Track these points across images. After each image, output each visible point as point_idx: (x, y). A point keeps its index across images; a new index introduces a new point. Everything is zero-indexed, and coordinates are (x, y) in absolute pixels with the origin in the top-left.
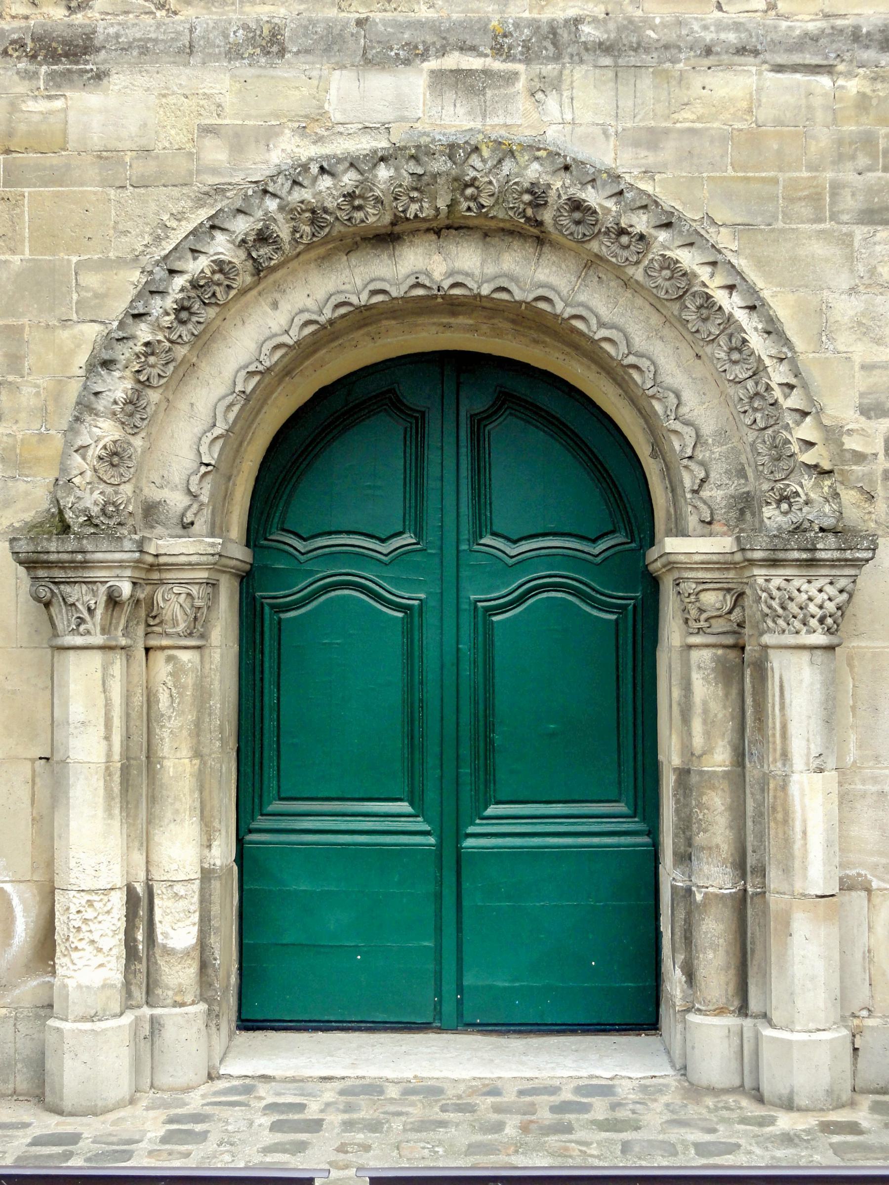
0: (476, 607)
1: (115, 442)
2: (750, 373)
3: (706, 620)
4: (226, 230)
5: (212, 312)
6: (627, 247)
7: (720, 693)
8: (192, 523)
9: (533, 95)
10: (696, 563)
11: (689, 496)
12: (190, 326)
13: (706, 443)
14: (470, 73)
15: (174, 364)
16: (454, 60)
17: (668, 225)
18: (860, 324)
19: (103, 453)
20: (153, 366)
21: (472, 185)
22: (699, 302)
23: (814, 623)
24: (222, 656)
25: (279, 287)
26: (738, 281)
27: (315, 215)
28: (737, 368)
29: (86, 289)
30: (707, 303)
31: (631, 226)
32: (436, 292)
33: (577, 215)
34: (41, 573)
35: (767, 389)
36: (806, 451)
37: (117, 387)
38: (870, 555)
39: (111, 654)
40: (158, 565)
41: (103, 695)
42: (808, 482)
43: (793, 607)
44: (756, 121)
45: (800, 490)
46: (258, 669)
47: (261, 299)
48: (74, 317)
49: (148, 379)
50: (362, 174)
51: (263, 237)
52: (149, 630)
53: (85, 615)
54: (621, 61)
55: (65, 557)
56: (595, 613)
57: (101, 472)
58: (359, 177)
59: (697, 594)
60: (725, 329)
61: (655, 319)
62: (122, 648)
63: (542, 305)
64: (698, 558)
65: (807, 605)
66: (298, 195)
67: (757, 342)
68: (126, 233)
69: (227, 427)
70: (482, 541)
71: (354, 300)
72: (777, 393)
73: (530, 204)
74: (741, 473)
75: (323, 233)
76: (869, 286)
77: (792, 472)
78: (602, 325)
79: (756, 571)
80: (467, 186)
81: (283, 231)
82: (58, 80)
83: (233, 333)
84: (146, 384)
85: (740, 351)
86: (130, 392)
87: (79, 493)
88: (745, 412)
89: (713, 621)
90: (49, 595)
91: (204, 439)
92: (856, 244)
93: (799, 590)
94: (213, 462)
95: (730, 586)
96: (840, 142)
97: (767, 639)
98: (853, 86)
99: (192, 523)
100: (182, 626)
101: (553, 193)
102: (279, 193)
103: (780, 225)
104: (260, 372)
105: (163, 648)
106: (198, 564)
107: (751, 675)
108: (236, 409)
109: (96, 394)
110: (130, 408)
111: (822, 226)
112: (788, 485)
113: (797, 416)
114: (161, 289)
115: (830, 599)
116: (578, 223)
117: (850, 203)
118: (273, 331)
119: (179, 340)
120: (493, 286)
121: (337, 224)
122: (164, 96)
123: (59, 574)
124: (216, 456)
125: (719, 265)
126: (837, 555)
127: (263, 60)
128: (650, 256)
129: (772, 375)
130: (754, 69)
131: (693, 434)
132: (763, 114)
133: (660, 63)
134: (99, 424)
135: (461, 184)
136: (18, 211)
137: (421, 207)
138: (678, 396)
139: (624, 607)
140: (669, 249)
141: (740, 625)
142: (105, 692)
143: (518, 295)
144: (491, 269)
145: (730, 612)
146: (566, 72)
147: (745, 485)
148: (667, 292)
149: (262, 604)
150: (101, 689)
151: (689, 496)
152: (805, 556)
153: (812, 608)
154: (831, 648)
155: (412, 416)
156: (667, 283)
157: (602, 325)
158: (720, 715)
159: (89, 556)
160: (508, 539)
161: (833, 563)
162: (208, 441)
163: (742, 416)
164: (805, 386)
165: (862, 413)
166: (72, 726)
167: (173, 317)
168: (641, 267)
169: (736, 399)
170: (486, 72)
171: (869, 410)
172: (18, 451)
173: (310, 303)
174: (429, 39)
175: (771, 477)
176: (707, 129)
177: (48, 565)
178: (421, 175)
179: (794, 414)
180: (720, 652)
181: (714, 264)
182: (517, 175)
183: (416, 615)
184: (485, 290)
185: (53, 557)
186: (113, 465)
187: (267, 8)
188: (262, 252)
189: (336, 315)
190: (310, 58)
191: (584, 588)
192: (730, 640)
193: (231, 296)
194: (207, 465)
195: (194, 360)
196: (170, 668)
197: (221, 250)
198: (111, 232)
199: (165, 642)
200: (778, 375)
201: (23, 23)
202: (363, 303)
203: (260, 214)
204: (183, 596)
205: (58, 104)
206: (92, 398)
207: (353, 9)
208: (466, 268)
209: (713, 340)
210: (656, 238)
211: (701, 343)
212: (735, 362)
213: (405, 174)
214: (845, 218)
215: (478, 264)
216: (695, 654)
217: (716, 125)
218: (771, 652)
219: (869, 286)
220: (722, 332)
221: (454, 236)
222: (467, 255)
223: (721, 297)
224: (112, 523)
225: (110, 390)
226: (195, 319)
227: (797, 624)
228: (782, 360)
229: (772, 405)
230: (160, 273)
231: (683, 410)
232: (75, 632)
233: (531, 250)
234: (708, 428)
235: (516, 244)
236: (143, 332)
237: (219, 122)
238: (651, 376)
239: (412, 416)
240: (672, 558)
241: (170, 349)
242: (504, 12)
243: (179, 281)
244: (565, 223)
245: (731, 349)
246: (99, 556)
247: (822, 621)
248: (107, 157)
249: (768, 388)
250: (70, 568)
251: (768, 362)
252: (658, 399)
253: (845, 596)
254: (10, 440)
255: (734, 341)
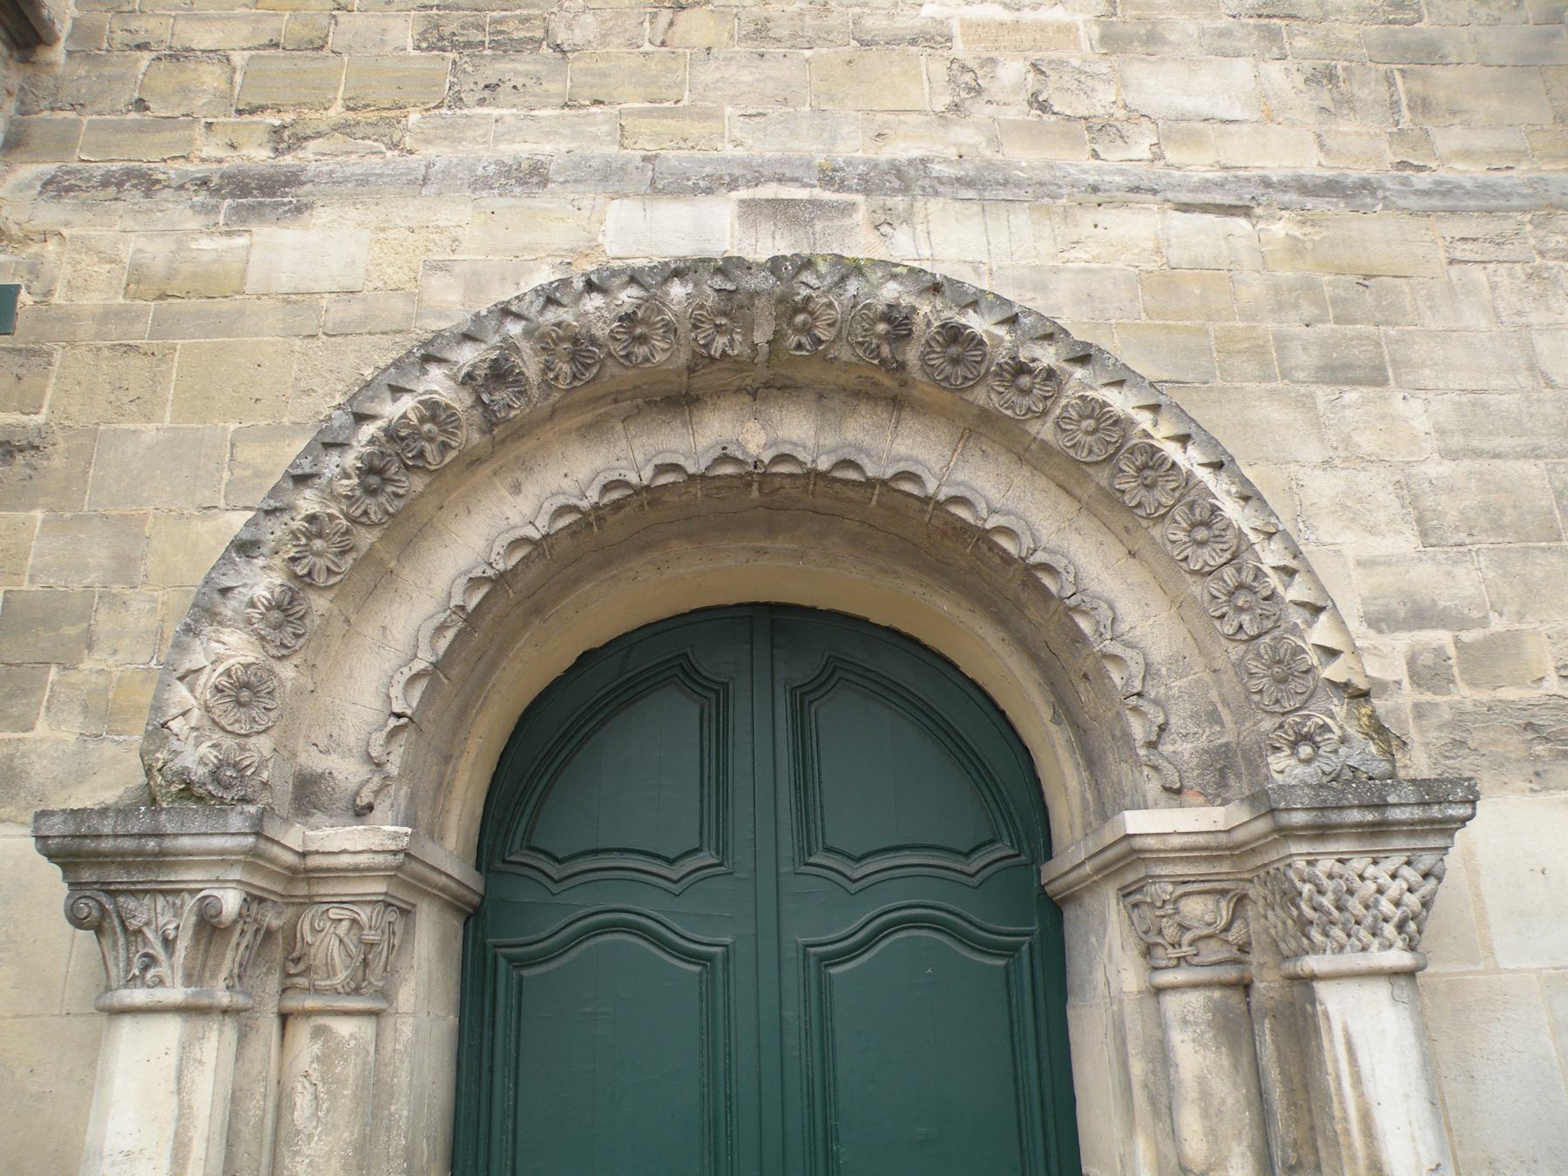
0: (805, 954)
1: (247, 666)
2: (1228, 555)
3: (1192, 943)
4: (445, 361)
5: (418, 483)
6: (1026, 392)
7: (1226, 1063)
8: (370, 808)
9: (877, 227)
10: (1174, 850)
11: (1142, 752)
12: (382, 499)
13: (1158, 674)
14: (791, 203)
15: (354, 555)
16: (768, 191)
17: (1083, 359)
18: (1345, 507)
19: (224, 681)
20: (318, 554)
21: (804, 310)
22: (1140, 460)
23: (1389, 930)
24: (416, 1031)
25: (524, 464)
26: (1193, 430)
27: (579, 346)
28: (1205, 553)
29: (245, 466)
30: (1152, 463)
31: (1034, 360)
32: (751, 469)
33: (954, 350)
34: (87, 876)
35: (1256, 578)
36: (1328, 663)
37: (262, 582)
38: (1469, 811)
39: (200, 1023)
40: (307, 871)
41: (175, 1099)
42: (1340, 708)
43: (1354, 905)
44: (1168, 263)
45: (1329, 721)
46: (486, 1053)
47: (496, 480)
48: (222, 504)
49: (309, 574)
50: (647, 290)
51: (500, 373)
52: (288, 982)
53: (158, 950)
54: (987, 195)
55: (128, 844)
56: (965, 953)
57: (217, 711)
58: (642, 293)
59: (1176, 901)
60: (1182, 495)
61: (1066, 505)
62: (225, 1011)
63: (908, 487)
64: (1177, 841)
65: (1377, 901)
66: (552, 315)
67: (1231, 509)
68: (308, 392)
69: (433, 659)
70: (812, 860)
71: (633, 478)
72: (1274, 580)
73: (886, 337)
74: (1214, 717)
75: (588, 376)
76: (1346, 459)
77: (1311, 696)
78: (993, 511)
79: (1295, 848)
80: (797, 310)
81: (530, 365)
82: (246, 215)
83: (453, 527)
84: (306, 581)
85: (1207, 525)
86: (278, 590)
87: (176, 745)
88: (1222, 616)
89: (1202, 945)
90: (95, 913)
91: (398, 677)
92: (1321, 407)
93: (1362, 877)
94: (409, 712)
95: (1224, 885)
96: (1276, 289)
97: (1311, 963)
98: (1280, 228)
99: (370, 808)
100: (342, 975)
101: (919, 319)
102: (526, 313)
103: (1219, 382)
104: (489, 579)
105: (308, 1014)
106: (370, 869)
107: (1272, 1030)
108: (450, 634)
109: (225, 591)
110: (276, 615)
111: (1273, 385)
112: (1308, 717)
113: (1306, 614)
114: (340, 439)
115: (1410, 890)
116: (955, 361)
117: (1303, 359)
118: (512, 522)
119: (364, 519)
120: (834, 459)
121: (609, 362)
122: (383, 230)
123: (117, 876)
124: (414, 704)
125: (1164, 410)
126: (1418, 813)
127: (518, 190)
128: (1064, 402)
129: (1261, 554)
130: (1155, 207)
131: (1141, 661)
132: (1175, 256)
133: (1037, 198)
134: (224, 638)
135: (789, 308)
136: (164, 367)
137: (732, 341)
138: (1112, 608)
139: (1016, 948)
140: (1091, 388)
141: (1244, 948)
142: (179, 1091)
143: (872, 471)
144: (829, 440)
145: (1227, 929)
146: (919, 204)
147: (1222, 734)
148: (1090, 452)
149: (495, 956)
150: (173, 1087)
151: (1142, 752)
152: (1370, 817)
153: (1386, 906)
154: (1410, 974)
155: (710, 689)
156: (1090, 438)
157: (993, 511)
158: (1230, 1101)
159: (168, 843)
160: (850, 857)
161: (1414, 828)
162: (403, 679)
163: (1217, 623)
164: (1310, 571)
165: (1370, 626)
166: (107, 1161)
167: (356, 481)
168: (1050, 423)
169: (1207, 597)
170: (811, 202)
171: (1379, 620)
172: (111, 695)
173: (567, 484)
174: (737, 172)
175: (1277, 708)
176: (1108, 270)
177: (99, 859)
178: (731, 292)
179: (1301, 610)
180: (1217, 994)
181: (1155, 408)
182: (868, 295)
183: (720, 966)
184: (824, 464)
185: (106, 845)
186: (240, 704)
187: (527, 146)
188: (497, 396)
189: (606, 500)
190: (581, 187)
191: (959, 921)
192: (1230, 973)
193: (448, 459)
194: (399, 716)
195: (393, 564)
196: (317, 1048)
197: (436, 388)
198: (289, 391)
199: (311, 1003)
200: (1271, 556)
201: (215, 166)
202: (645, 482)
203: (495, 340)
204: (345, 924)
205: (242, 241)
206: (217, 597)
207: (638, 146)
208: (795, 438)
209: (1163, 516)
210: (1071, 375)
211: (1145, 523)
212: (1202, 544)
213: (709, 291)
214: (1301, 375)
215: (812, 433)
216: (1172, 1003)
217: (1119, 265)
218: (1323, 990)
219: (1346, 459)
220: (1179, 500)
221: (776, 398)
222: (795, 421)
223: (1172, 451)
224: (228, 796)
225: (245, 585)
226: (390, 489)
227: (1364, 934)
228: (1270, 536)
229: (1265, 599)
230: (341, 418)
231: (1123, 627)
232: (131, 982)
233: (885, 415)
234: (1159, 652)
235: (863, 408)
236: (308, 502)
237: (453, 257)
238: (1071, 579)
239: (710, 689)
240: (1138, 843)
241: (348, 532)
242: (830, 151)
243: (369, 430)
244: (937, 362)
245: (1194, 525)
246: (186, 843)
247: (1401, 927)
248: (296, 300)
249: (1259, 574)
250: (137, 865)
251: (1253, 537)
252: (1085, 613)
253: (1432, 882)
254: (102, 680)
255: (1197, 511)
